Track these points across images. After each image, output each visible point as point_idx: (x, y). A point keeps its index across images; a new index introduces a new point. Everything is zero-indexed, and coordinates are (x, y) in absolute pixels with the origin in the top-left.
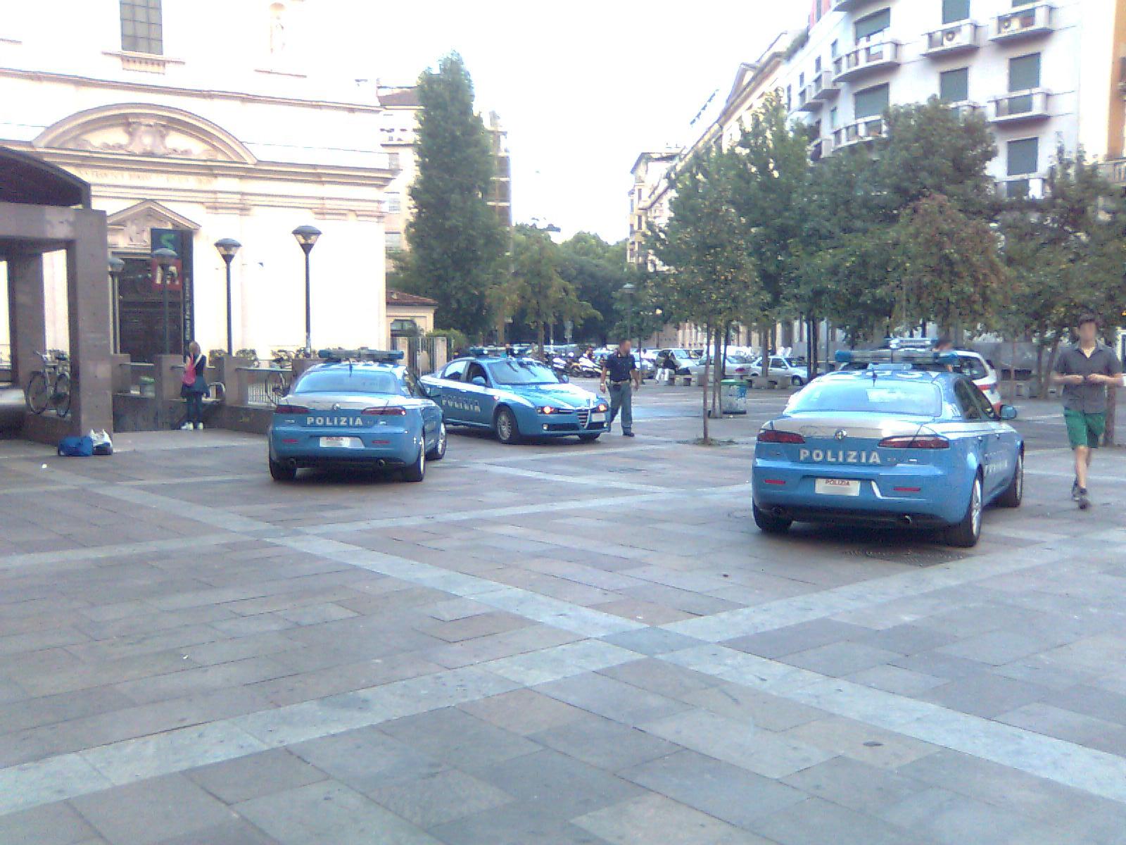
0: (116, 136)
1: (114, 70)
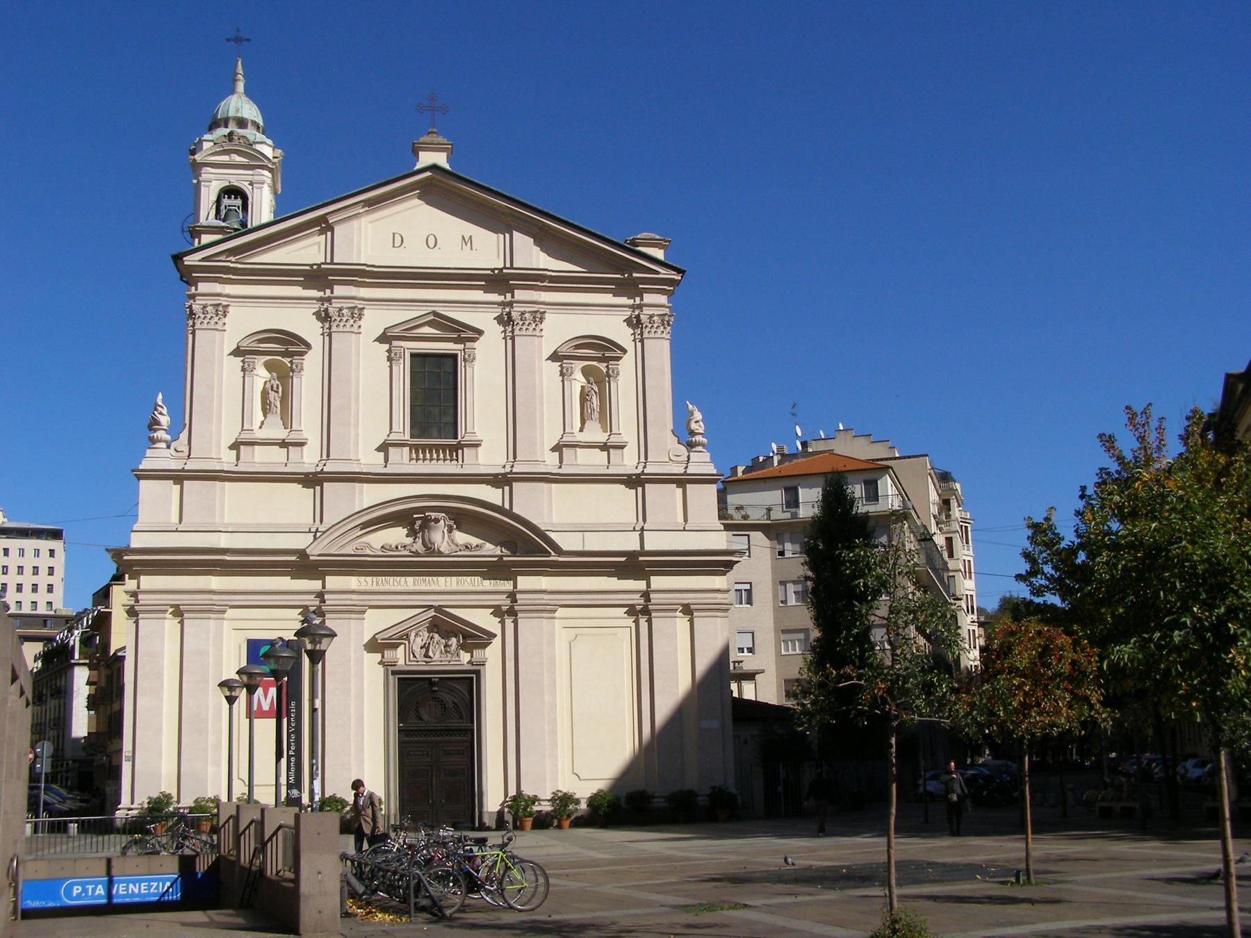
0: (397, 535)
1: (402, 461)
